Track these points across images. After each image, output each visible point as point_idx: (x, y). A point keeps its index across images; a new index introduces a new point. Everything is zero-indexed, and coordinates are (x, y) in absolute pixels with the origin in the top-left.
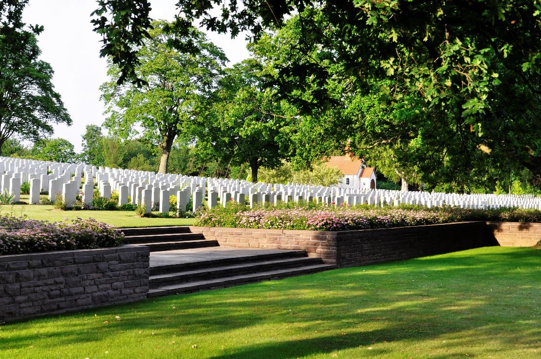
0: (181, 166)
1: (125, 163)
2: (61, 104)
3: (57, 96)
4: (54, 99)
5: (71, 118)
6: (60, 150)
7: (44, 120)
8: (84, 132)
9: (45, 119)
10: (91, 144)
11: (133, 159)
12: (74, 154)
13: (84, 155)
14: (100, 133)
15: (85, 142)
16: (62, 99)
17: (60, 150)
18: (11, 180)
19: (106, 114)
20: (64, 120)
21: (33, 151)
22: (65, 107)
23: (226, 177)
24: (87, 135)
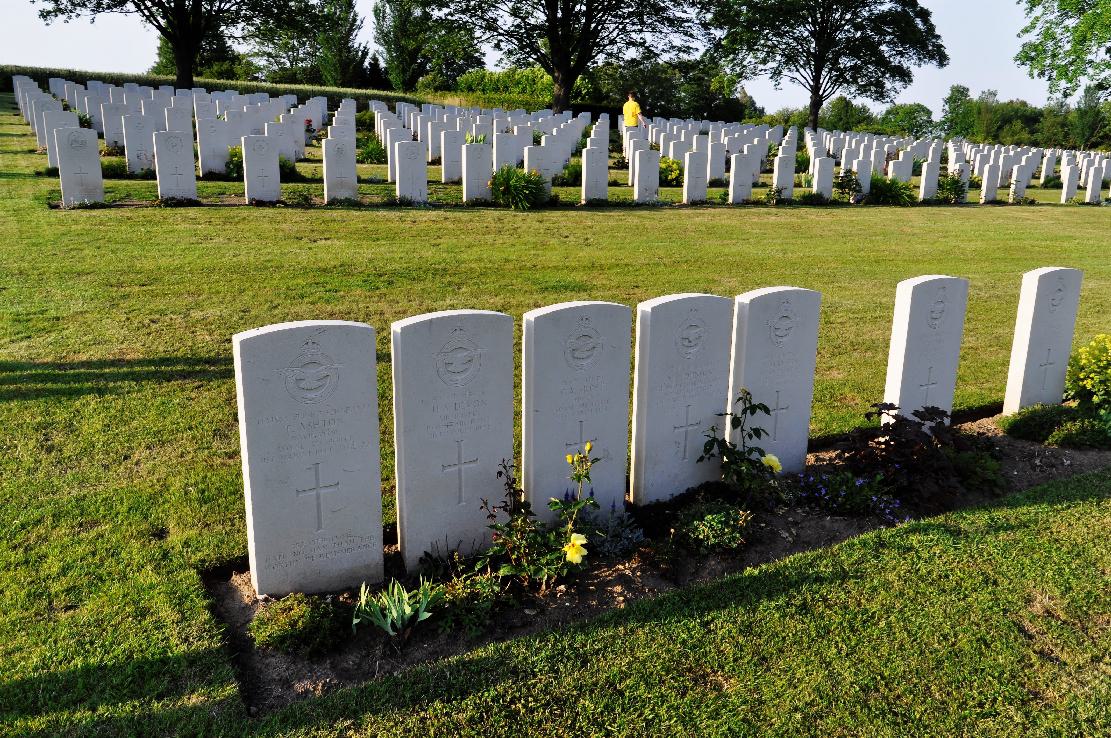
0: (1084, 135)
1: (995, 137)
2: (931, 28)
3: (925, 15)
4: (918, 21)
5: (947, 52)
6: (915, 118)
7: (895, 61)
8: (947, 94)
9: (898, 57)
10: (954, 109)
11: (1007, 127)
12: (931, 121)
13: (944, 123)
14: (967, 96)
15: (947, 107)
16: (933, 20)
17: (915, 118)
18: (862, 145)
19: (1027, 35)
20: (932, 57)
21: (884, 119)
22: (937, 32)
23: (447, 86)
24: (950, 98)
